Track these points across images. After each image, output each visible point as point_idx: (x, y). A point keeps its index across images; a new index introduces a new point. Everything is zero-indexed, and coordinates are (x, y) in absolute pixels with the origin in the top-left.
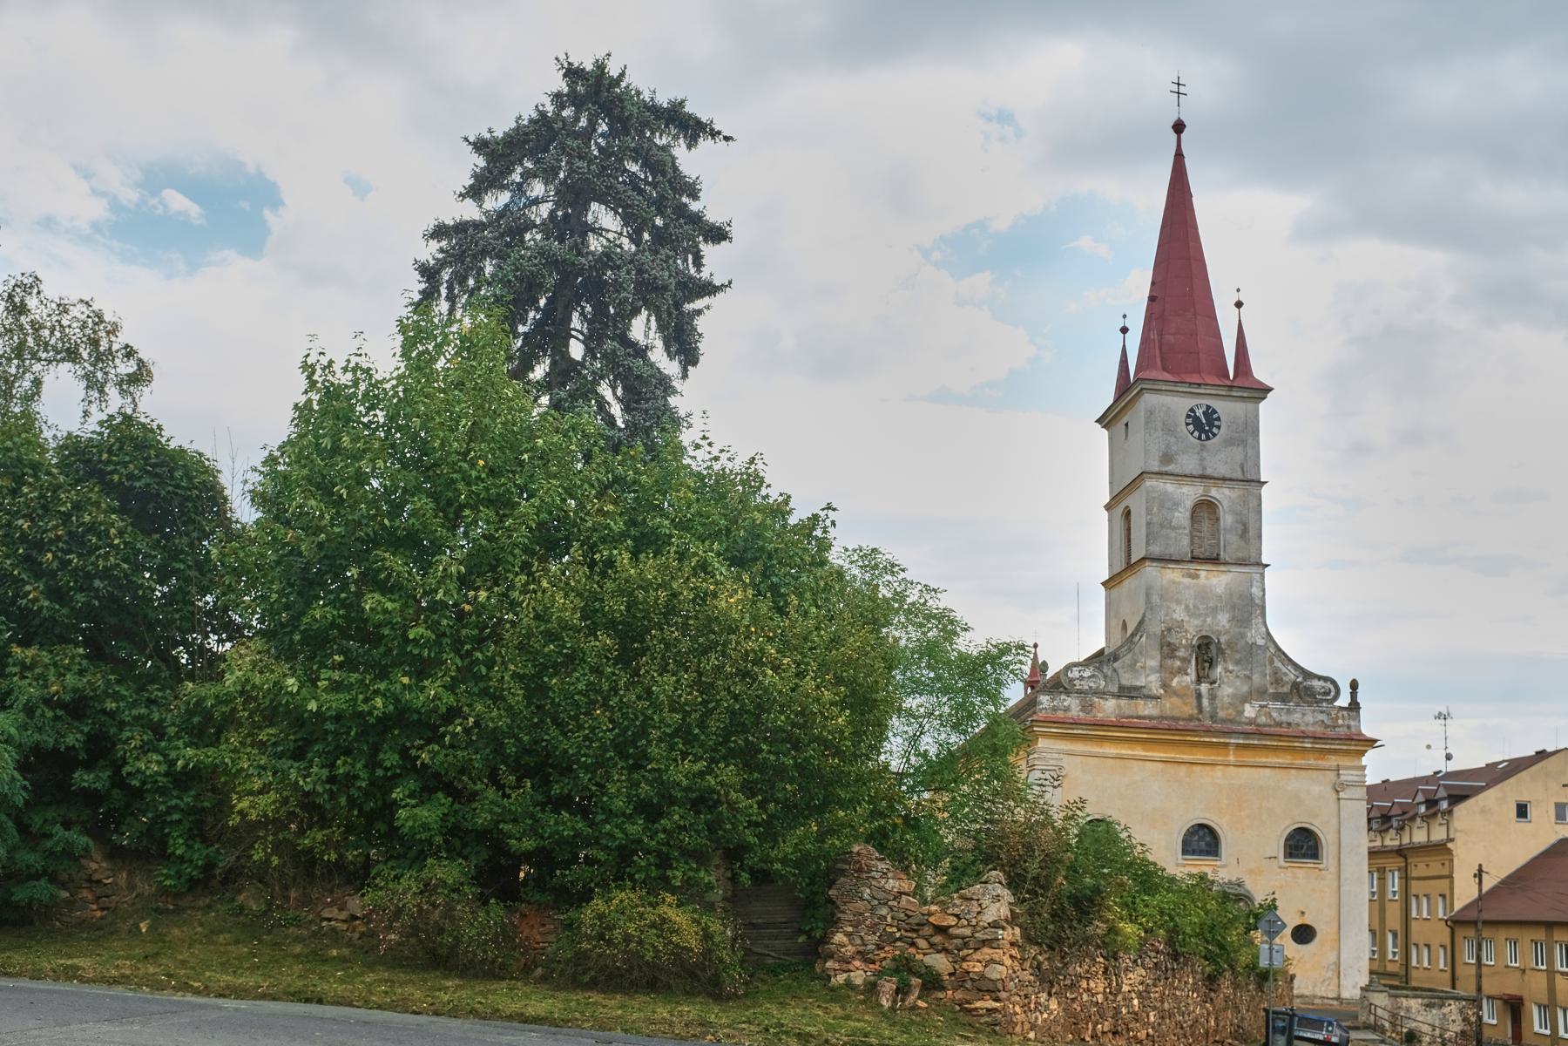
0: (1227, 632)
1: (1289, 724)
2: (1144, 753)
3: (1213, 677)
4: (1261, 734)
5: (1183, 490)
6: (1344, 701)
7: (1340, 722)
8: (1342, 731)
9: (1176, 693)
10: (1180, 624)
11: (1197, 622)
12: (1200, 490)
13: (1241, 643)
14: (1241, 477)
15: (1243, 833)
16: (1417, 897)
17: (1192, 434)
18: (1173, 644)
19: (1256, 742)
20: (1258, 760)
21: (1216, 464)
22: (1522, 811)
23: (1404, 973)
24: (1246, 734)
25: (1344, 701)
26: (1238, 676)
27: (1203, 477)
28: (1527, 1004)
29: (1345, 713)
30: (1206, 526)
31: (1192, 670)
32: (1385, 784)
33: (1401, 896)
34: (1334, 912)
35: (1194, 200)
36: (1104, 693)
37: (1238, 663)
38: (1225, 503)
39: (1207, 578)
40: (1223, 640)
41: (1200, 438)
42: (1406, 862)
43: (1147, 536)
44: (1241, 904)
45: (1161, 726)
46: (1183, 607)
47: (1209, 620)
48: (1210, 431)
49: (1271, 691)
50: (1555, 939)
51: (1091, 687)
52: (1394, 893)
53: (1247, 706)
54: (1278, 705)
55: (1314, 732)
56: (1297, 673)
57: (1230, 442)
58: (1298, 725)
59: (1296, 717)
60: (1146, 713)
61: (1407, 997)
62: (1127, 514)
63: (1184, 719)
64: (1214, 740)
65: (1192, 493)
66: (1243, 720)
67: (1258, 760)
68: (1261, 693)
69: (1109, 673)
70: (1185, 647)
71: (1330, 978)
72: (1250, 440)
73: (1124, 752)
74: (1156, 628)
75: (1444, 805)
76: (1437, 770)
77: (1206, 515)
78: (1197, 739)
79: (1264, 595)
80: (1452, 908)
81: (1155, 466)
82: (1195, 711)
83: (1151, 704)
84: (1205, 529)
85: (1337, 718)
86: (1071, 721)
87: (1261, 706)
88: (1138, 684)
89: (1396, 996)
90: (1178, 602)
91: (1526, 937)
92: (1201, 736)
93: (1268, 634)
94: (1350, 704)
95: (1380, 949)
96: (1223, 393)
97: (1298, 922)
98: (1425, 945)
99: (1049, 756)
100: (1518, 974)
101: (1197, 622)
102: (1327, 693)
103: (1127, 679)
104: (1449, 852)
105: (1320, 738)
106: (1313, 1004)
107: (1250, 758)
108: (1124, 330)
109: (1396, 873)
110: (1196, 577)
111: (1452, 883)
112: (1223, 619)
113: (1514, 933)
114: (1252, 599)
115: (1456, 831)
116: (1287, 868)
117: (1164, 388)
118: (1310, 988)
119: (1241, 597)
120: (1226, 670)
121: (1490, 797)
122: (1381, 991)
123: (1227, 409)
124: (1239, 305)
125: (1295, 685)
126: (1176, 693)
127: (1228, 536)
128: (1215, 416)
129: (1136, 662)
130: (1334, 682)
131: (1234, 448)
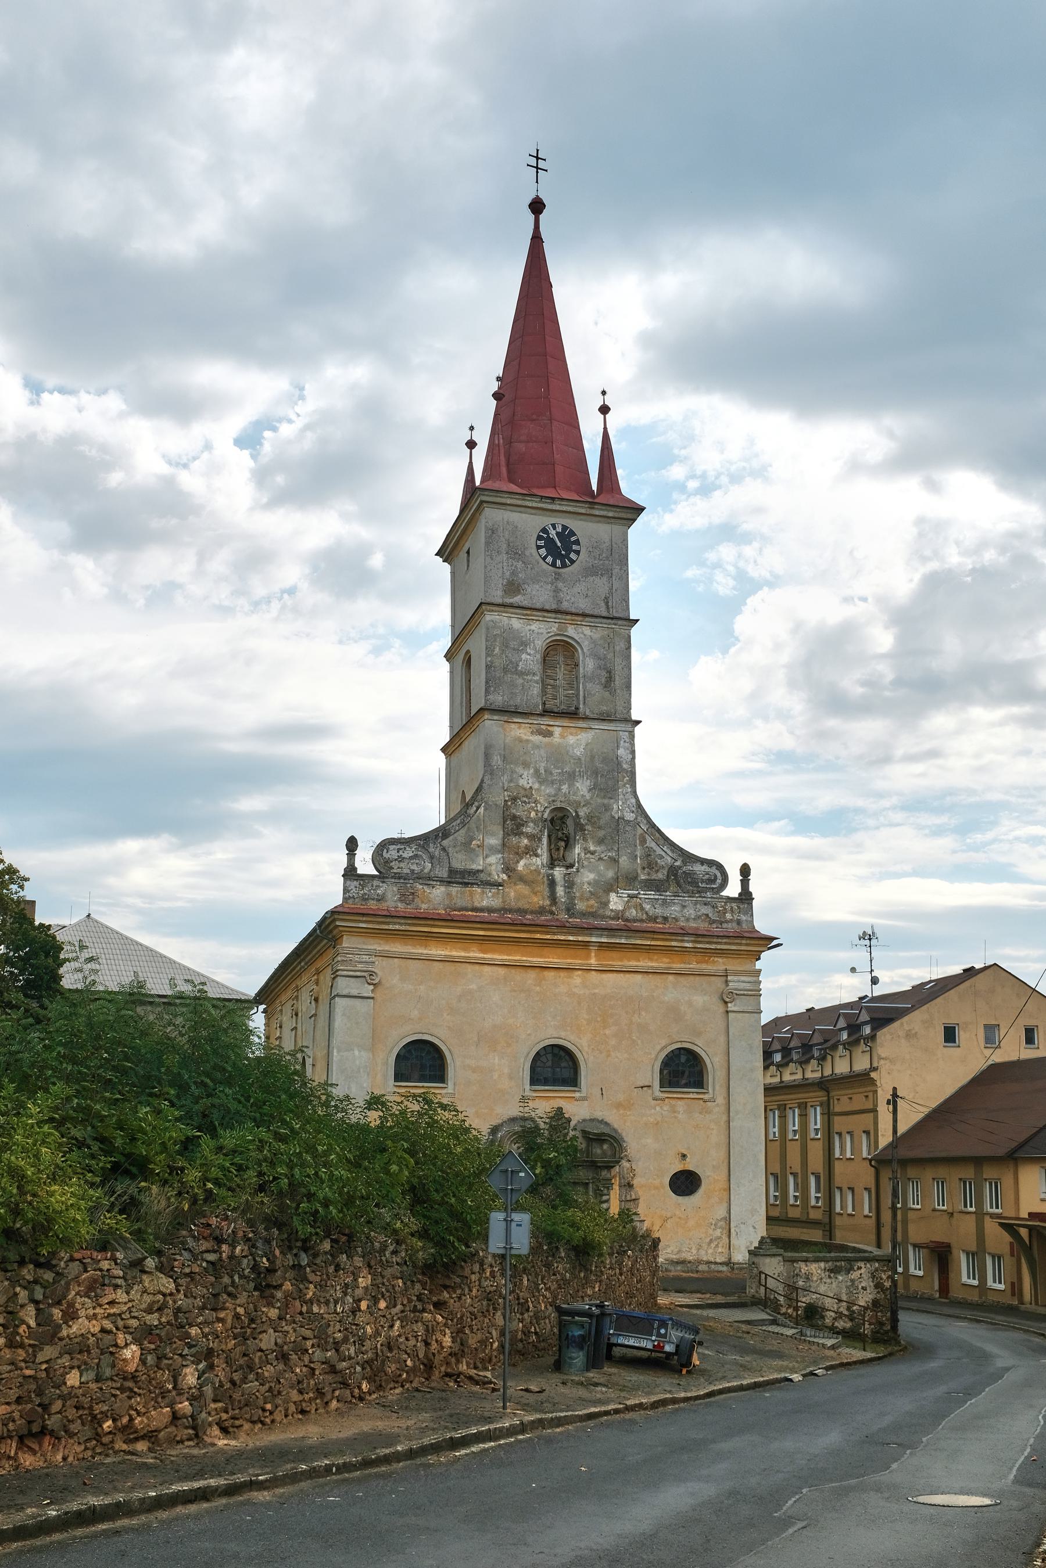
0: (587, 803)
1: (665, 919)
2: (481, 955)
3: (569, 860)
4: (629, 930)
5: (533, 627)
6: (733, 889)
7: (728, 916)
8: (731, 927)
9: (522, 879)
10: (528, 793)
11: (550, 790)
12: (554, 628)
13: (605, 819)
14: (605, 614)
15: (608, 1056)
16: (840, 1134)
17: (544, 559)
18: (519, 817)
19: (623, 941)
20: (626, 963)
21: (575, 598)
22: (950, 1035)
23: (827, 1220)
24: (611, 931)
25: (733, 889)
26: (600, 859)
27: (557, 611)
28: (955, 1251)
29: (734, 905)
30: (561, 673)
31: (543, 850)
32: (809, 1013)
33: (823, 1135)
34: (722, 1154)
35: (553, 289)
36: (430, 879)
37: (601, 842)
38: (586, 644)
39: (562, 736)
40: (583, 812)
41: (554, 565)
42: (828, 1096)
43: (487, 682)
44: (605, 1147)
45: (502, 921)
46: (532, 771)
47: (565, 788)
48: (567, 556)
49: (643, 877)
50: (984, 1177)
51: (413, 871)
52: (817, 1130)
53: (613, 896)
54: (652, 894)
55: (697, 929)
56: (674, 856)
57: (591, 571)
58: (676, 919)
59: (674, 910)
60: (485, 903)
61: (806, 1260)
62: (468, 662)
63: (532, 912)
64: (571, 938)
65: (545, 631)
66: (608, 913)
67: (626, 963)
68: (631, 880)
69: (437, 853)
70: (534, 821)
71: (720, 1238)
72: (616, 570)
73: (454, 953)
74: (498, 797)
75: (867, 1030)
76: (863, 995)
77: (562, 659)
78: (548, 937)
79: (634, 758)
80: (876, 1147)
81: (497, 596)
82: (548, 902)
83: (490, 892)
84: (560, 676)
85: (725, 912)
86: (385, 913)
87: (630, 896)
88: (474, 867)
89: (793, 1261)
90: (526, 765)
91: (954, 1175)
92: (554, 934)
93: (639, 806)
94: (740, 894)
95: (802, 1194)
96: (583, 511)
97: (678, 1167)
98: (849, 1188)
99: (356, 958)
100: (946, 1217)
101: (550, 790)
102: (713, 881)
103: (460, 861)
104: (873, 1082)
105: (703, 936)
106: (697, 1272)
107: (617, 961)
108: (471, 444)
109: (818, 1108)
110: (550, 734)
111: (876, 1119)
112: (582, 787)
113: (942, 1171)
114: (619, 764)
115: (880, 1058)
116: (663, 1100)
117: (509, 501)
118: (694, 1251)
119: (605, 760)
120: (587, 851)
121: (914, 1021)
122: (774, 1255)
123: (585, 530)
124: (604, 410)
125: (673, 871)
126: (522, 879)
127: (589, 685)
128: (573, 539)
129: (472, 839)
130: (720, 867)
131: (597, 580)
